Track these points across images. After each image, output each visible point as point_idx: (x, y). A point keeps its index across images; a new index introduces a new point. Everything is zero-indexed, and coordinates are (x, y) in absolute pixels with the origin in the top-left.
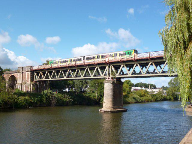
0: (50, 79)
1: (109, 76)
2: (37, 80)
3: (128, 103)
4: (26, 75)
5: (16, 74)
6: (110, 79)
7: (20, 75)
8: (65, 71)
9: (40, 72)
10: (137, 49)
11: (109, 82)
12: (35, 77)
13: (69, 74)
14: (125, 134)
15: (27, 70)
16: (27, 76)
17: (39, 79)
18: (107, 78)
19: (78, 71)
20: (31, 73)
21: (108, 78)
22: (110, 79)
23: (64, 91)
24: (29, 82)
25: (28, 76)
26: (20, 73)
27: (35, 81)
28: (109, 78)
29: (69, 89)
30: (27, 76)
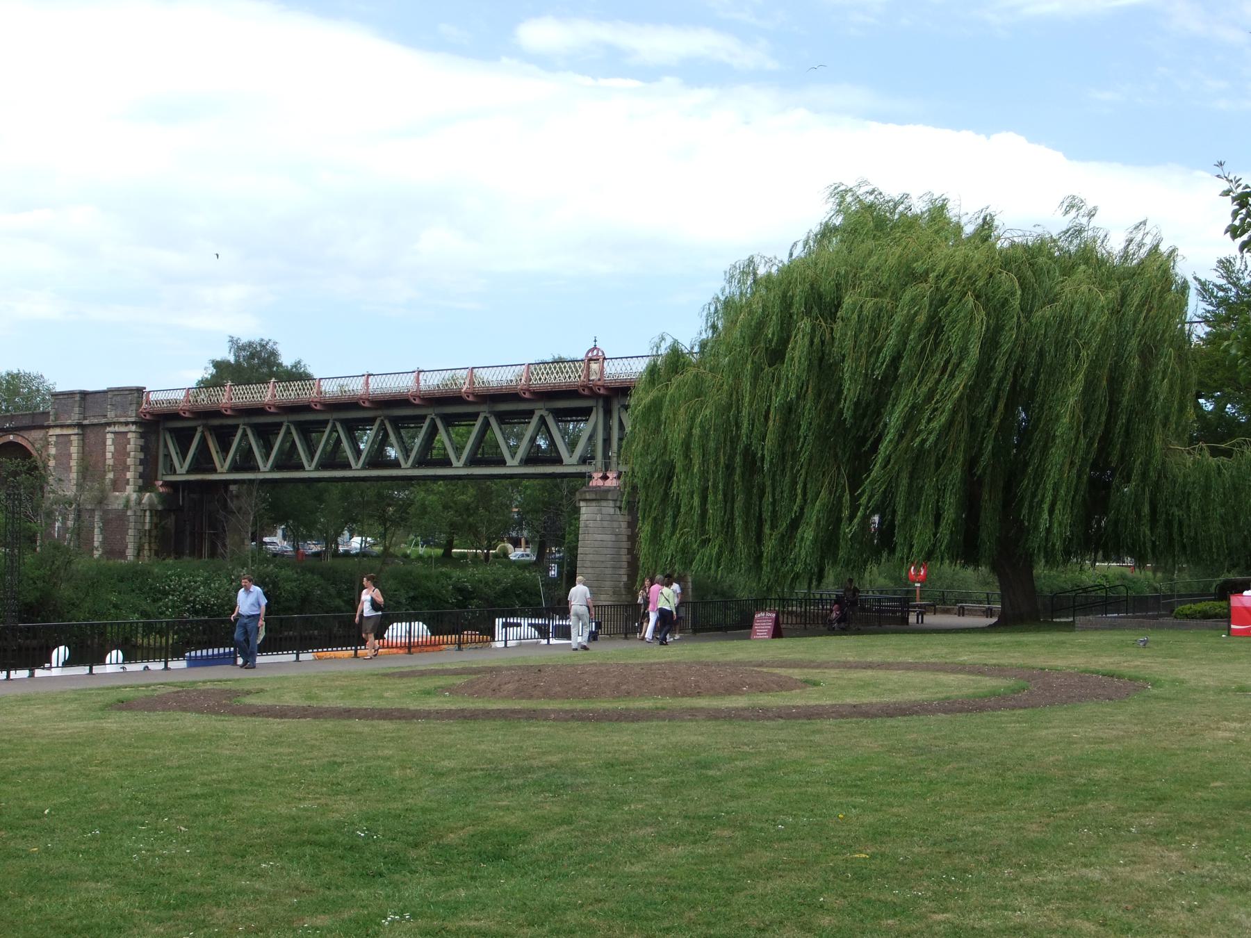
0: (265, 471)
1: (607, 467)
2: (182, 473)
3: (1206, 320)
4: (109, 442)
5: (36, 434)
6: (609, 483)
7: (64, 441)
8: (308, 430)
9: (200, 429)
10: (1064, 937)
11: (601, 496)
12: (168, 456)
13: (203, 449)
14: (731, 587)
15: (111, 415)
16: (110, 448)
17: (188, 472)
18: (597, 475)
19: (486, 424)
20: (142, 435)
21: (601, 475)
22: (609, 483)
23: (1202, 401)
24: (130, 489)
25: (121, 453)
26: (70, 431)
27: (166, 484)
28: (605, 478)
29: (294, 536)
30: (110, 448)
